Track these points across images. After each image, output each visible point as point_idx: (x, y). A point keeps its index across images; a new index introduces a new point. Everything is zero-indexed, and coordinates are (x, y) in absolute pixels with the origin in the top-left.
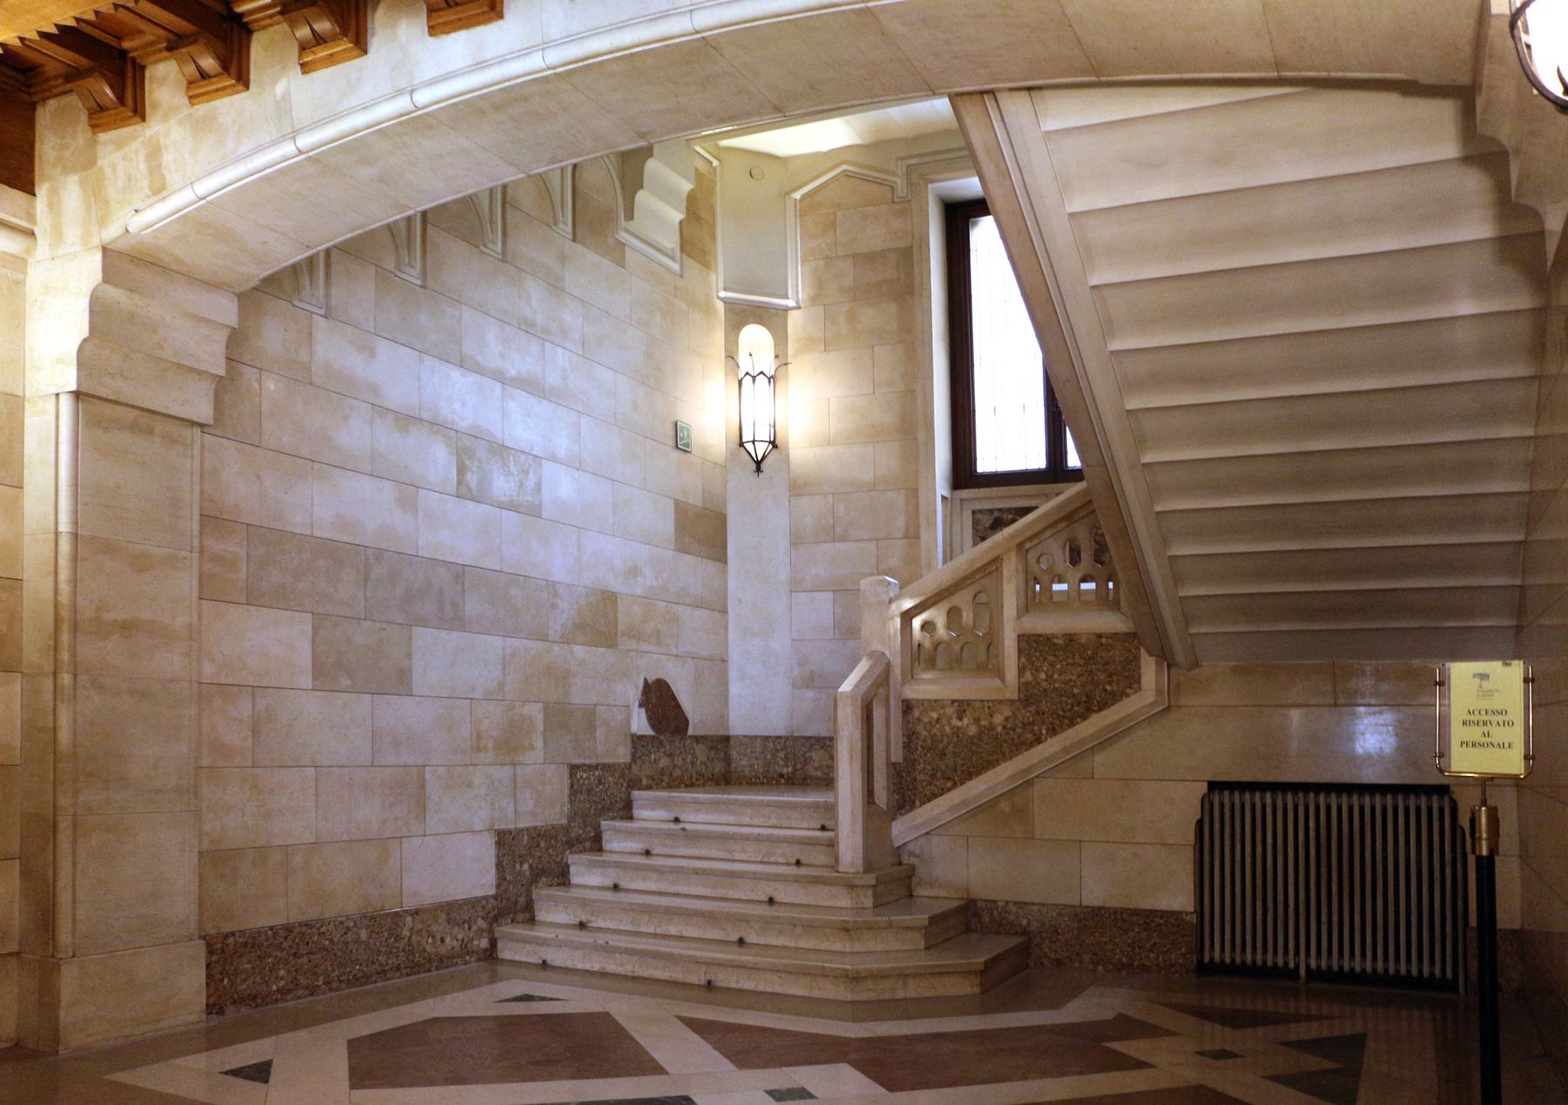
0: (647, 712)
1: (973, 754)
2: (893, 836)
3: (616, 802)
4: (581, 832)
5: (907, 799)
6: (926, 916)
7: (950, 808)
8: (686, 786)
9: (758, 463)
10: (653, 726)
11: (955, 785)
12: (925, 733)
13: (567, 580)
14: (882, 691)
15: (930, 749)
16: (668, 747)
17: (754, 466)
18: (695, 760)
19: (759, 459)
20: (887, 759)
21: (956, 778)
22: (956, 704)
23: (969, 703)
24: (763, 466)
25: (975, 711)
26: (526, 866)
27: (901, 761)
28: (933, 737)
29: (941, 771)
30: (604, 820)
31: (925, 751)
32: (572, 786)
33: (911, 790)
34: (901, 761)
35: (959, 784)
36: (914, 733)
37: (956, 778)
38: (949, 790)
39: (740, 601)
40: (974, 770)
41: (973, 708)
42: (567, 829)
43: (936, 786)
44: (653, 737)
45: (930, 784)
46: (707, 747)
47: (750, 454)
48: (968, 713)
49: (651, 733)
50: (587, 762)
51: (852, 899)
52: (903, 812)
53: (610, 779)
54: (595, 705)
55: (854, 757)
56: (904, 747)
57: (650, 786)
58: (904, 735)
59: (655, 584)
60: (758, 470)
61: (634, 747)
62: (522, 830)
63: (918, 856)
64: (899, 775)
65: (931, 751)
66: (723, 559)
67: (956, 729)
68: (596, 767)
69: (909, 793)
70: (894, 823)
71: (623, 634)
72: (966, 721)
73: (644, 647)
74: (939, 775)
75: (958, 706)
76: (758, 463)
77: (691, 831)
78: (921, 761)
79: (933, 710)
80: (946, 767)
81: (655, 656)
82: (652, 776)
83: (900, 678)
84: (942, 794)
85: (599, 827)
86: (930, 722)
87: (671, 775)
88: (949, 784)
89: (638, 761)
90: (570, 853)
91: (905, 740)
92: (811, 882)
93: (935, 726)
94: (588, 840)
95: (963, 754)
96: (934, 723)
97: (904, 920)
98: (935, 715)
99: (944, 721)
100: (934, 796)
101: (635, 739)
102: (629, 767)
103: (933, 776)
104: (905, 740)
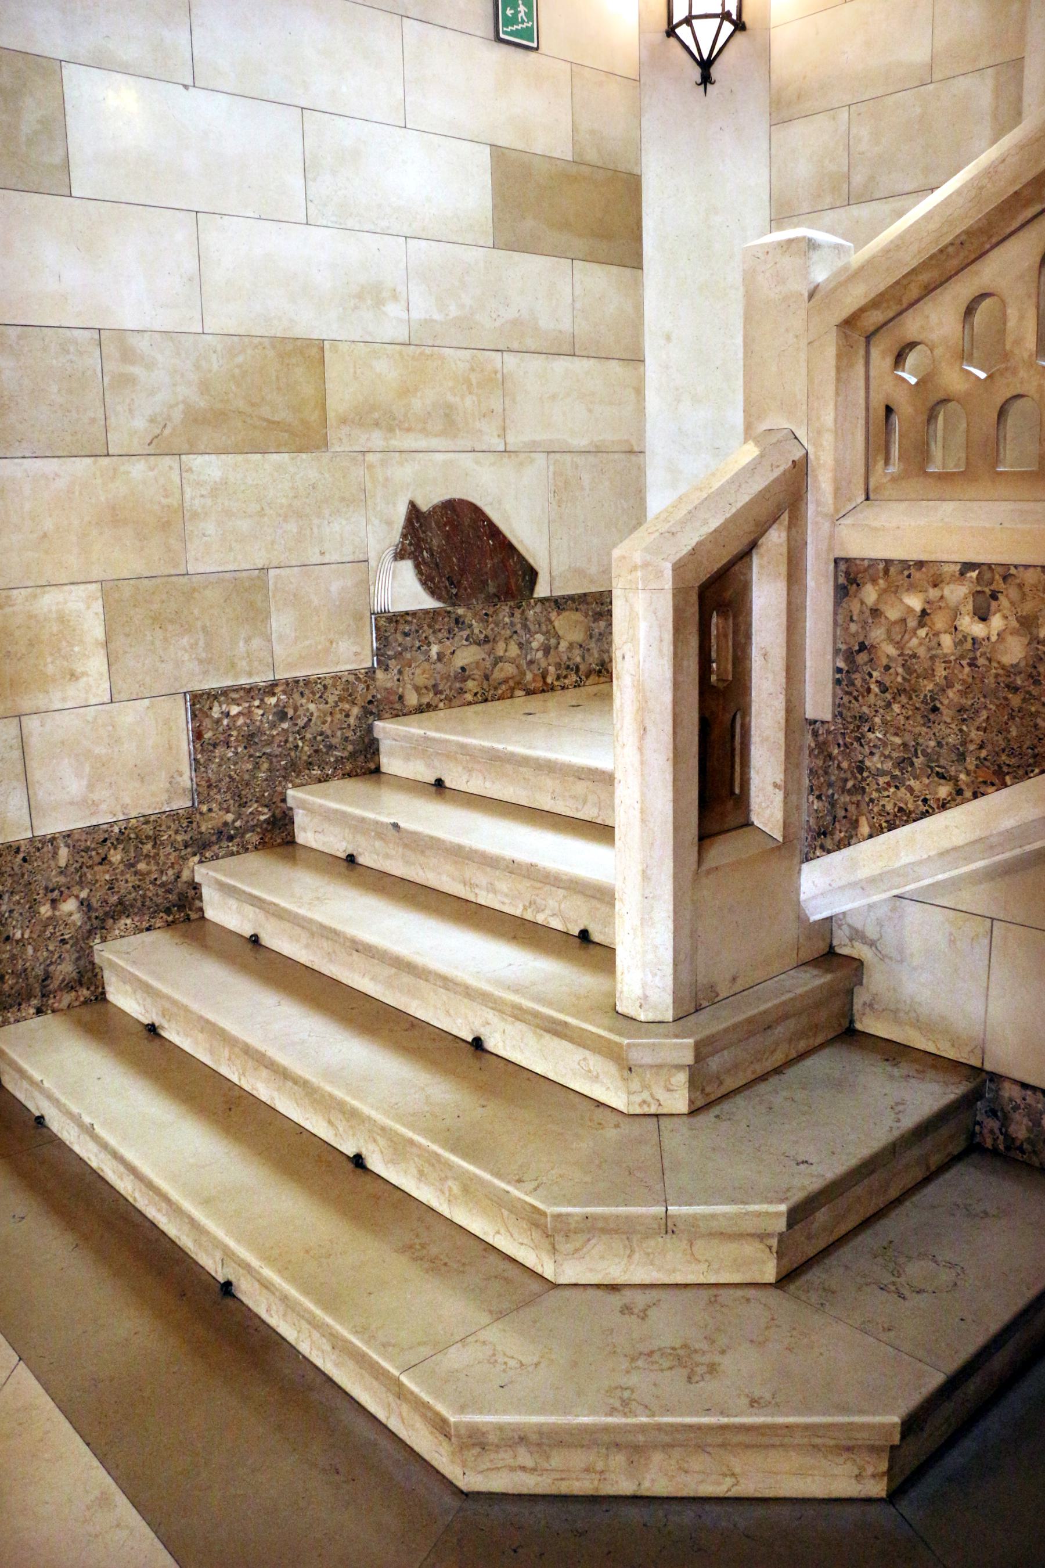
0: (417, 566)
1: (1012, 717)
2: (803, 897)
3: (330, 747)
4: (230, 817)
5: (841, 813)
6: (783, 1208)
7: (942, 854)
8: (529, 692)
9: (706, 65)
10: (433, 592)
11: (958, 796)
12: (891, 650)
13: (164, 321)
14: (776, 538)
15: (901, 691)
16: (477, 627)
17: (696, 73)
18: (553, 641)
19: (705, 56)
20: (789, 711)
21: (963, 777)
22: (974, 574)
23: (1007, 573)
24: (715, 71)
25: (1024, 597)
26: (69, 906)
27: (828, 717)
28: (908, 660)
29: (925, 753)
30: (295, 786)
31: (888, 696)
32: (198, 735)
33: (850, 792)
34: (828, 717)
35: (968, 794)
36: (862, 647)
37: (963, 777)
38: (944, 806)
39: (668, 338)
40: (1013, 761)
41: (1020, 586)
42: (188, 818)
43: (911, 790)
44: (434, 614)
45: (896, 782)
46: (586, 616)
47: (686, 48)
48: (1003, 600)
49: (428, 603)
50: (243, 681)
51: (630, 1093)
52: (828, 843)
53: (312, 707)
54: (264, 569)
55: (650, 727)
56: (838, 682)
57: (429, 705)
58: (836, 652)
59: (436, 316)
60: (706, 79)
61: (382, 637)
62: (53, 840)
63: (872, 944)
64: (821, 749)
65: (904, 699)
66: (633, 260)
67: (968, 645)
68: (271, 689)
69: (846, 798)
70: (805, 867)
71: (344, 421)
72: (997, 622)
73: (410, 441)
74: (918, 762)
75: (979, 578)
76: (706, 65)
77: (407, 831)
78: (877, 720)
79: (912, 588)
80: (939, 744)
81: (439, 457)
82: (435, 686)
83: (830, 501)
84: (925, 814)
85: (284, 800)
86: (904, 621)
87: (487, 677)
88: (944, 791)
89: (392, 663)
90: (201, 862)
91: (841, 664)
92: (548, 1031)
93: (914, 633)
94: (252, 829)
95: (984, 714)
96: (912, 623)
97: (713, 1216)
98: (915, 602)
99: (940, 621)
100: (903, 817)
101: (382, 622)
102: (371, 672)
103: (903, 763)
104: (841, 664)
